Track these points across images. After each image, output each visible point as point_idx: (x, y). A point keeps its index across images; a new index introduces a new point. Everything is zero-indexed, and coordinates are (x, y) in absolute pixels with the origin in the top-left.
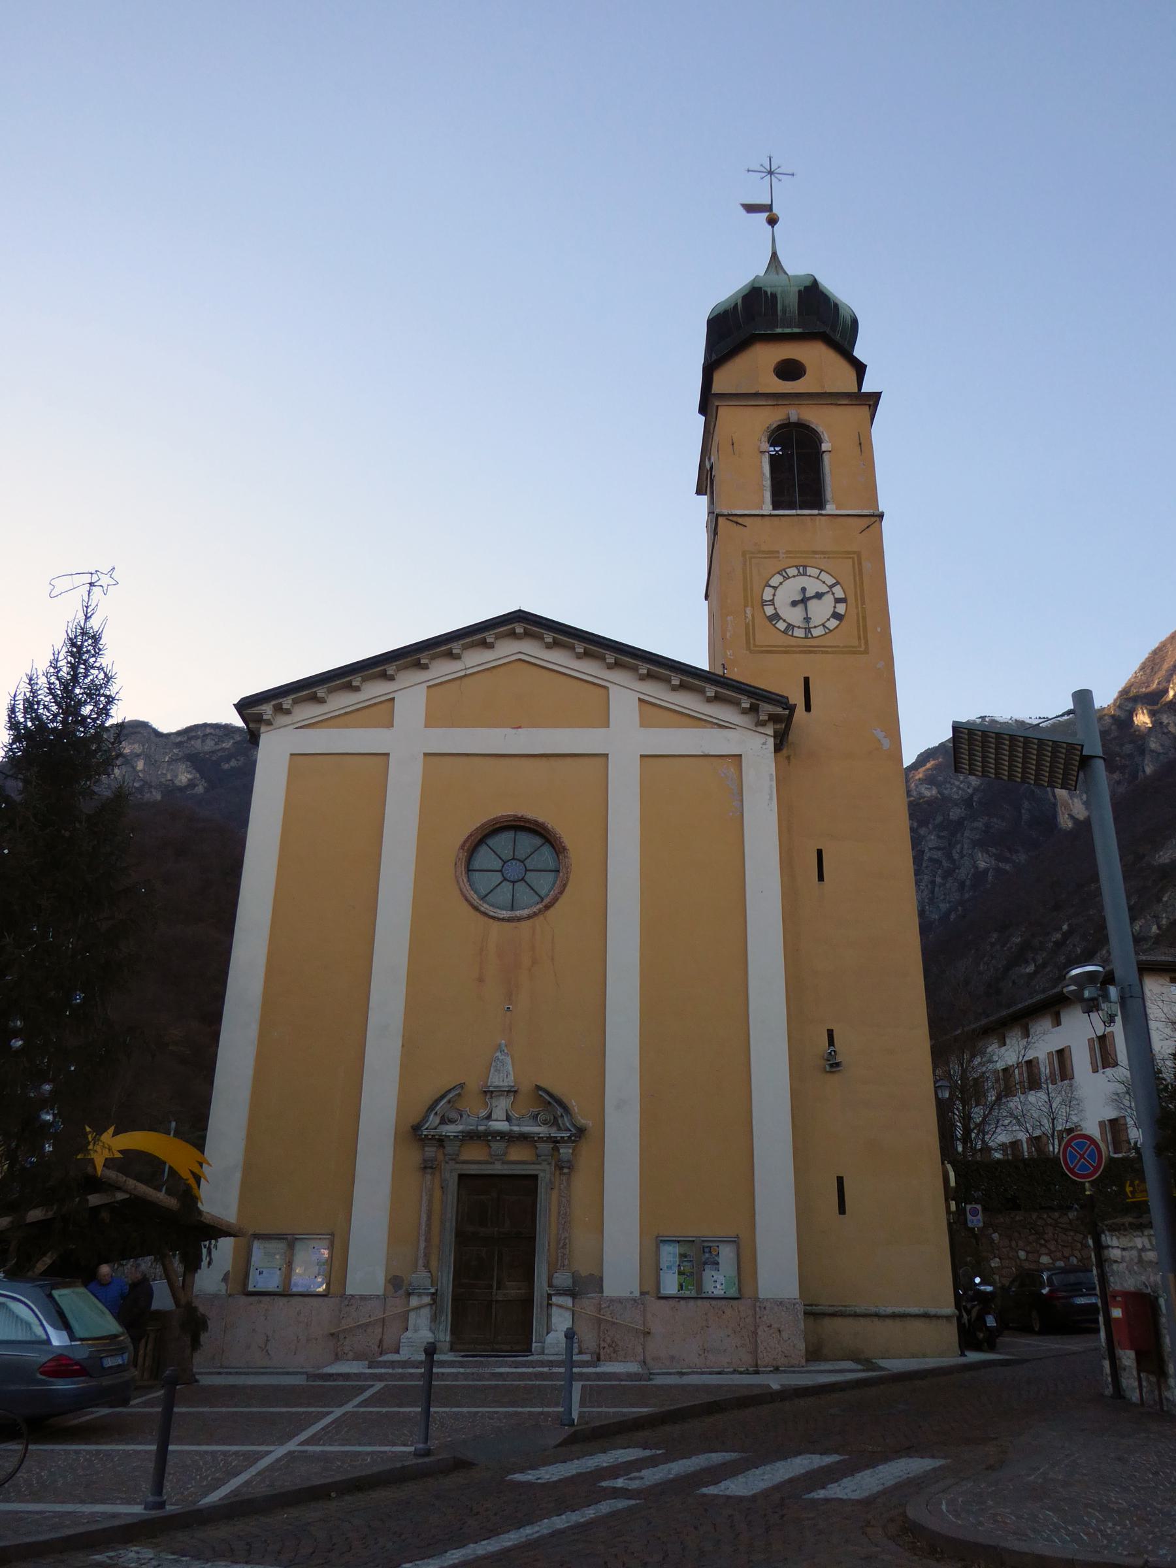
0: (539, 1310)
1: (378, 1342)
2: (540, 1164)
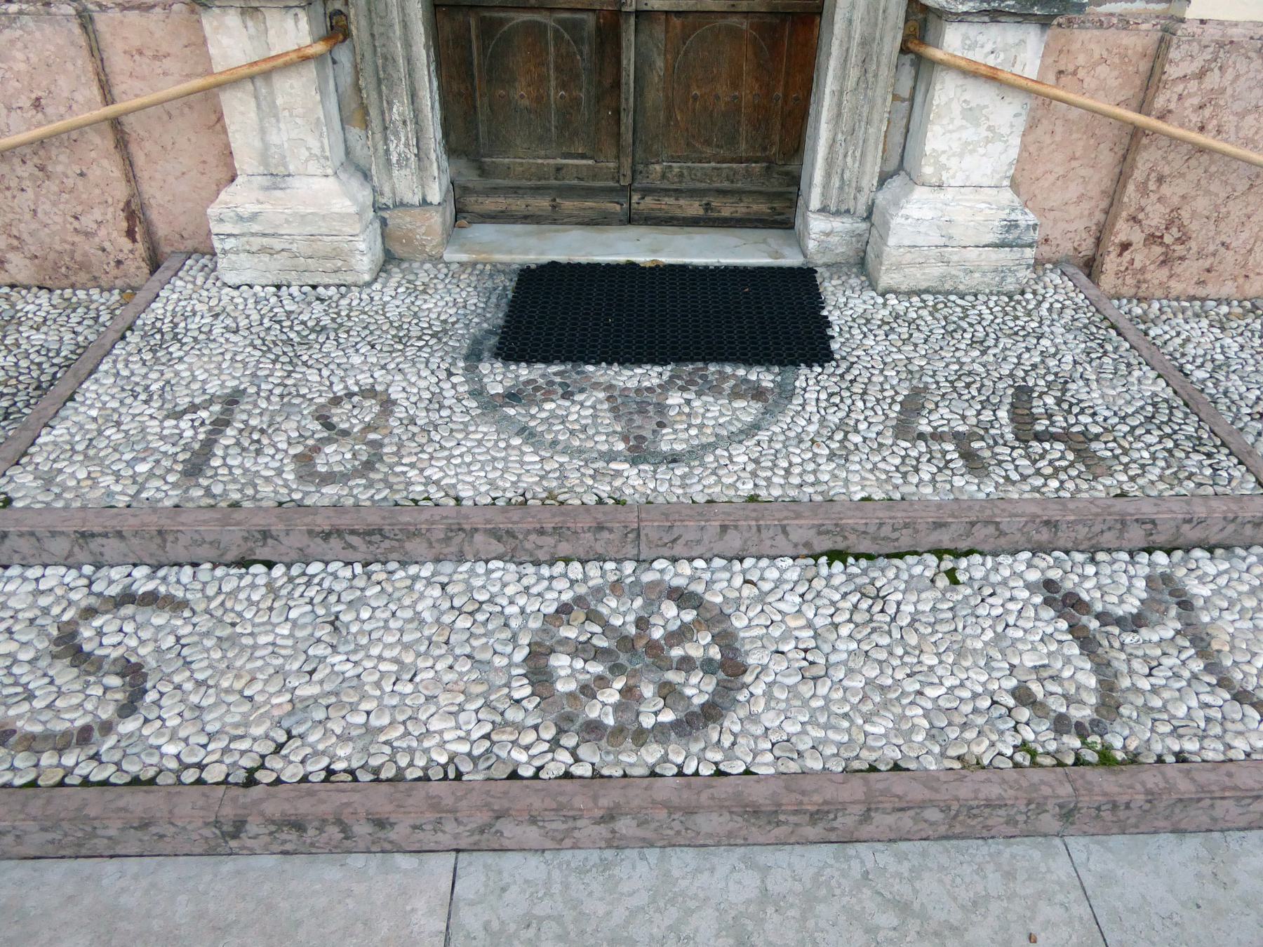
0: (854, 73)
1: (139, 174)
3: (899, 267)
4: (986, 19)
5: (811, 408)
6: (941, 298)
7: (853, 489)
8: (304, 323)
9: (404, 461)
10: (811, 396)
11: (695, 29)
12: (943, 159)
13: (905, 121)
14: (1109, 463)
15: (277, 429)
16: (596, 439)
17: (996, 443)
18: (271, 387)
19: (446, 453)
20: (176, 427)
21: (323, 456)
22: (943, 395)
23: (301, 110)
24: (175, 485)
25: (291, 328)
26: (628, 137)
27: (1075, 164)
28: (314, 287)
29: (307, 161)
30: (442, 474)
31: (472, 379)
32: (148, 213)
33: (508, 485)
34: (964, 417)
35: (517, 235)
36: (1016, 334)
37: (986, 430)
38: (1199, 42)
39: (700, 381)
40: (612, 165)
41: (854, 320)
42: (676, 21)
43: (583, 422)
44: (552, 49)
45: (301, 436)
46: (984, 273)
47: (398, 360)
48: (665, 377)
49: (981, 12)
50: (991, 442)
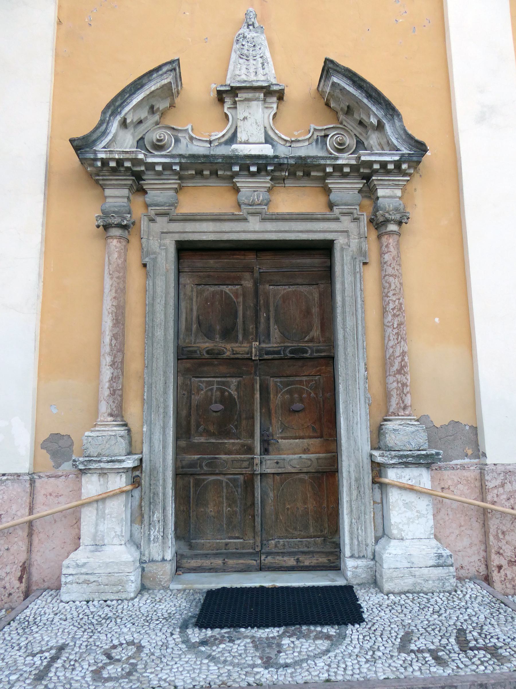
0: (355, 493)
1: (33, 549)
2: (337, 219)
3: (391, 579)
4: (403, 466)
5: (355, 642)
6: (415, 595)
7: (379, 674)
8: (100, 616)
9: (148, 671)
10: (355, 637)
11: (286, 480)
12: (400, 526)
13: (381, 512)
14: (508, 658)
15: (83, 660)
16: (247, 659)
17: (450, 652)
18: (81, 642)
19: (170, 667)
20: (32, 660)
21: (106, 670)
22: (421, 634)
23: (115, 515)
24: (29, 684)
25: (93, 618)
26: (258, 527)
27: (463, 528)
28: (106, 601)
29: (113, 538)
30: (167, 676)
31: (183, 636)
32: (31, 569)
33: (201, 679)
34: (432, 643)
35: (206, 577)
36: (455, 607)
37: (445, 647)
38: (496, 472)
39: (298, 634)
40: (251, 541)
41: (374, 605)
42: (277, 477)
43: (240, 652)
44: (225, 490)
45: (95, 662)
46: (434, 581)
47: (146, 629)
48: (280, 633)
49: (400, 463)
50: (448, 652)
